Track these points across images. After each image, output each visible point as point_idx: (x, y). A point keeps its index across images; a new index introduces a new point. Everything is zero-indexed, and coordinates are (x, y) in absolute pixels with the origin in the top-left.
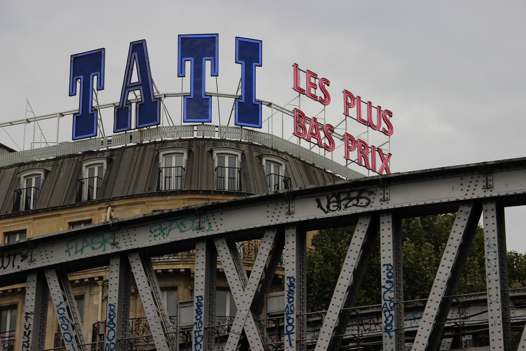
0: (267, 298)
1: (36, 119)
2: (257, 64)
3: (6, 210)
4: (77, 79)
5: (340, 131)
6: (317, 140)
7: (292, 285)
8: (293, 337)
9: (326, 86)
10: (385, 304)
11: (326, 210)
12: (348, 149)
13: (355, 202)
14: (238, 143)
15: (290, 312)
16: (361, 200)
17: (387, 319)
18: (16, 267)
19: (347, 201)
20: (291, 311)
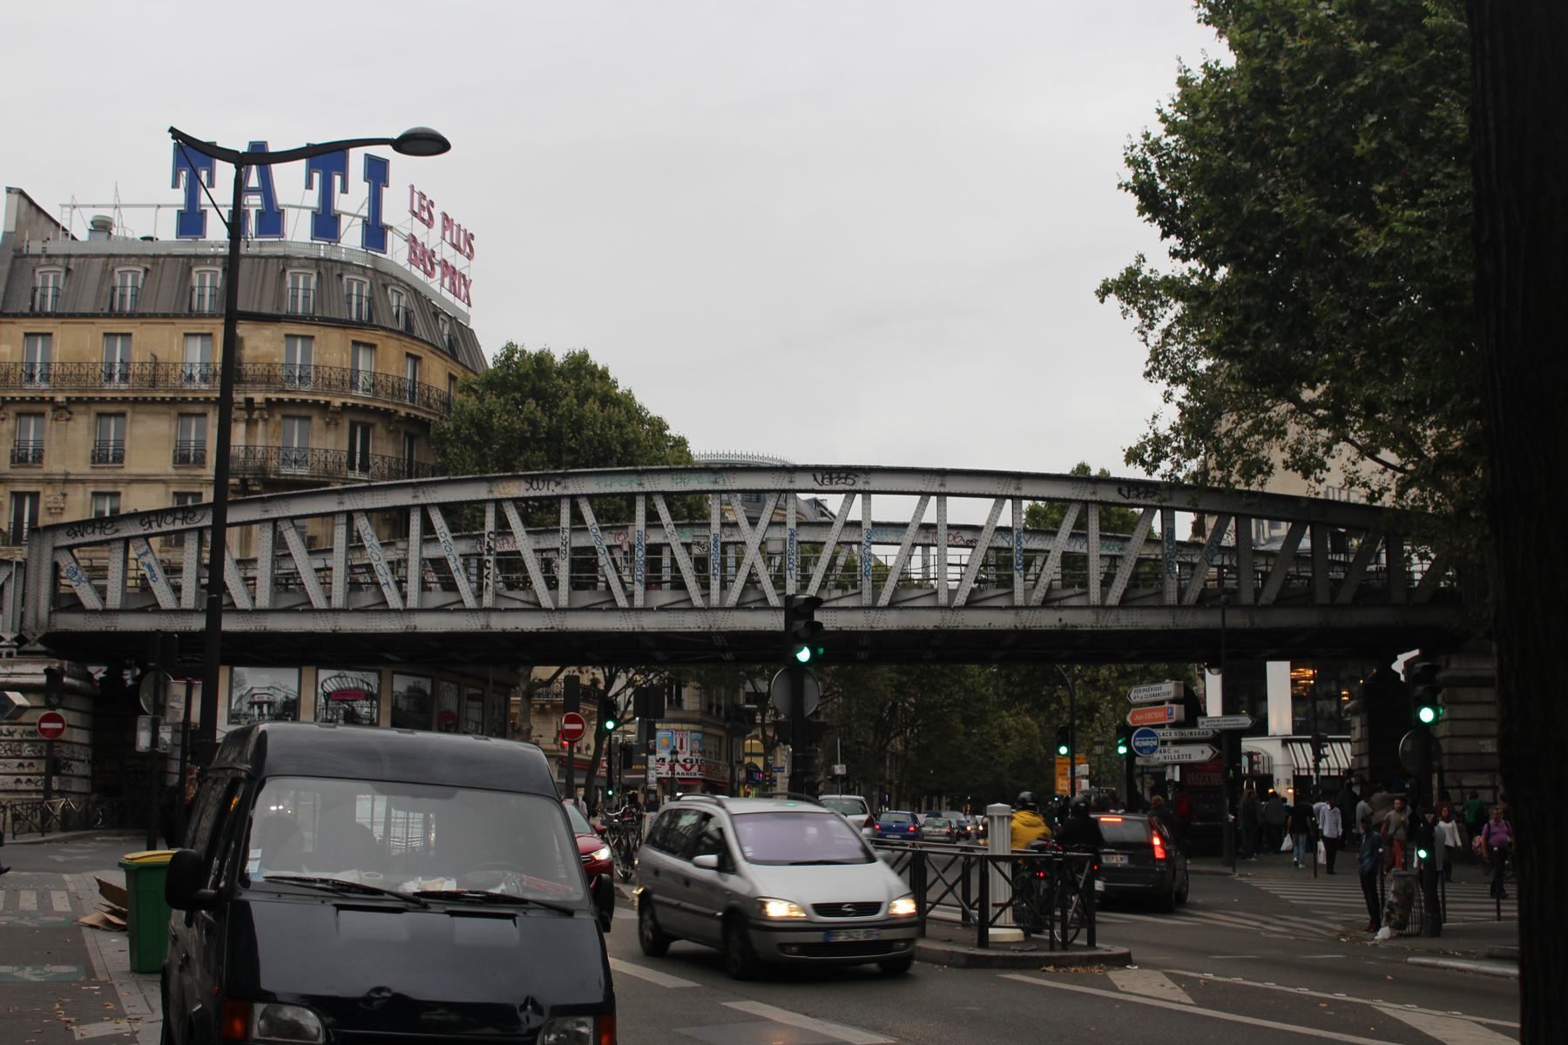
3: (101, 306)
5: (438, 257)
12: (443, 275)
14: (364, 267)
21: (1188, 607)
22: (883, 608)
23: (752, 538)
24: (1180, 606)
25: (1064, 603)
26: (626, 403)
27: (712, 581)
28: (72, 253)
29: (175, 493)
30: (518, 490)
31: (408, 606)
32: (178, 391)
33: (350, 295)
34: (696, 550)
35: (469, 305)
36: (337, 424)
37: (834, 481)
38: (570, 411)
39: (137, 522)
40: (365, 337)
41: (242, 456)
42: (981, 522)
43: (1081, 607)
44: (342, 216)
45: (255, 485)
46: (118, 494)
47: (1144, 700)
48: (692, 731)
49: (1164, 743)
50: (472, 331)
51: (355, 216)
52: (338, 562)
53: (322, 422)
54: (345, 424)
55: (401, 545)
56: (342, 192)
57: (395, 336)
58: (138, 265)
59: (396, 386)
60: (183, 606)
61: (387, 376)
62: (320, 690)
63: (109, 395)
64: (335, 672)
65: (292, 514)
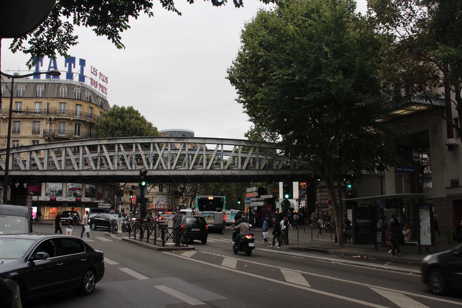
5: (98, 83)
12: (100, 87)
14: (79, 86)
21: (261, 170)
22: (190, 170)
23: (160, 154)
24: (259, 169)
25: (233, 169)
26: (143, 120)
27: (151, 164)
28: (8, 82)
29: (32, 141)
30: (105, 142)
31: (79, 169)
32: (33, 116)
33: (76, 93)
34: (147, 156)
35: (106, 94)
36: (72, 124)
38: (128, 121)
39: (16, 149)
40: (79, 103)
41: (49, 131)
42: (214, 149)
43: (237, 170)
45: (51, 139)
46: (18, 141)
47: (250, 191)
48: (165, 197)
49: (253, 201)
50: (107, 101)
51: (77, 73)
52: (63, 158)
53: (68, 123)
54: (74, 124)
55: (78, 155)
57: (86, 103)
58: (24, 85)
59: (86, 115)
60: (26, 169)
61: (84, 112)
62: (67, 188)
63: (16, 117)
64: (71, 184)
65: (52, 148)
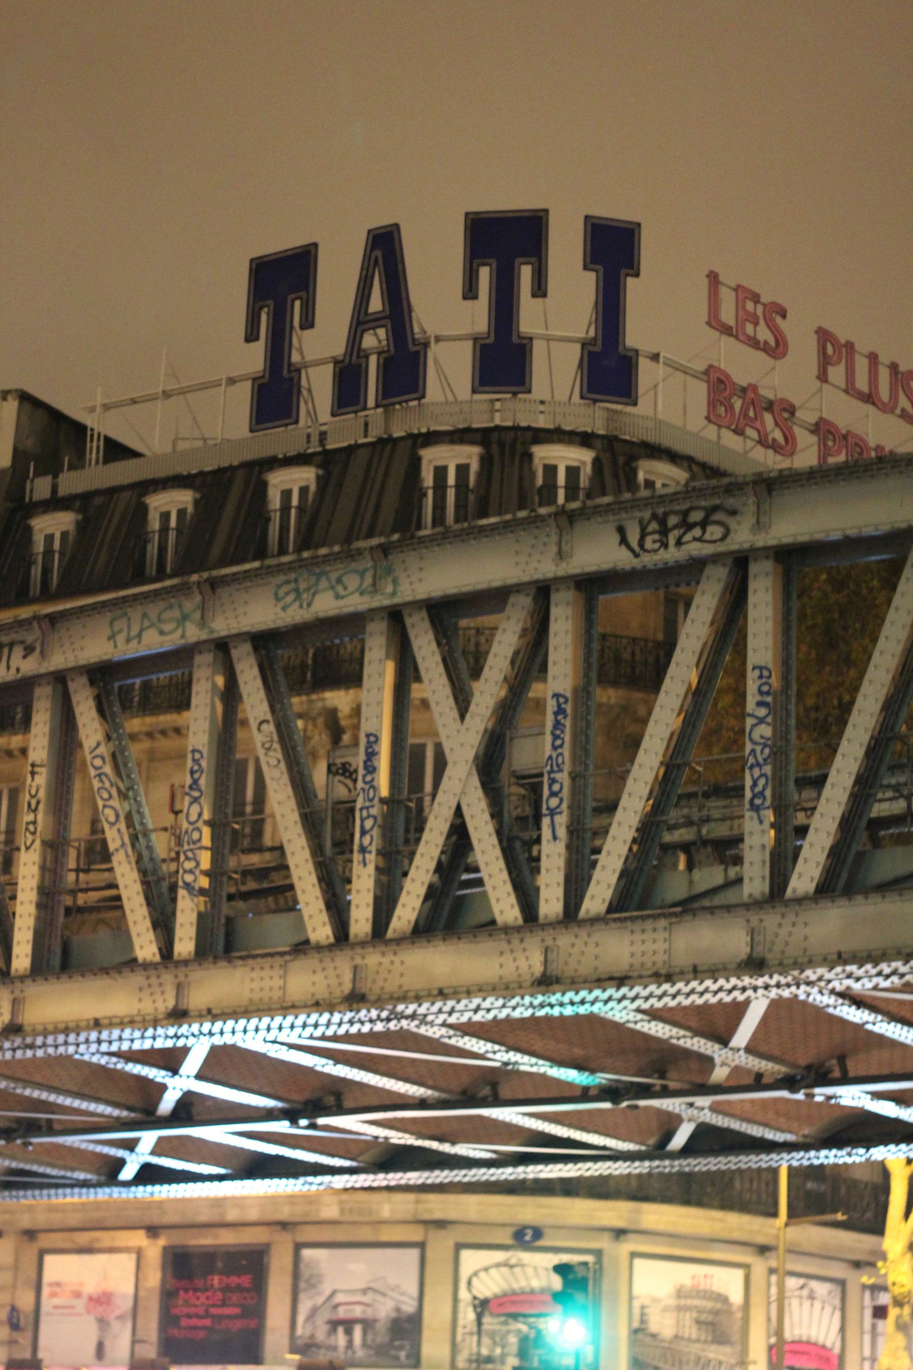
0: (511, 739)
1: (182, 392)
2: (631, 272)
4: (261, 308)
5: (806, 416)
6: (759, 432)
7: (560, 711)
8: (562, 820)
9: (779, 320)
10: (753, 751)
11: (637, 549)
13: (697, 532)
15: (555, 768)
16: (710, 529)
17: (755, 784)
18: (13, 670)
19: (682, 531)
20: (558, 765)
37: (672, 538)
44: (535, 342)
56: (534, 295)
62: (464, 1294)
